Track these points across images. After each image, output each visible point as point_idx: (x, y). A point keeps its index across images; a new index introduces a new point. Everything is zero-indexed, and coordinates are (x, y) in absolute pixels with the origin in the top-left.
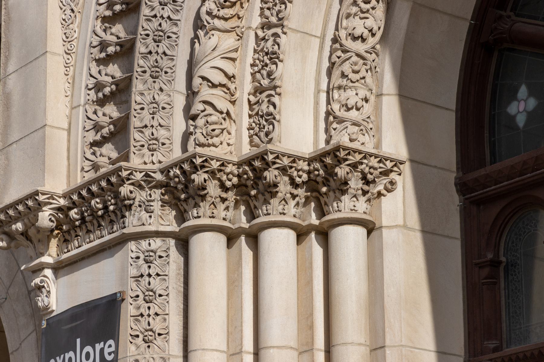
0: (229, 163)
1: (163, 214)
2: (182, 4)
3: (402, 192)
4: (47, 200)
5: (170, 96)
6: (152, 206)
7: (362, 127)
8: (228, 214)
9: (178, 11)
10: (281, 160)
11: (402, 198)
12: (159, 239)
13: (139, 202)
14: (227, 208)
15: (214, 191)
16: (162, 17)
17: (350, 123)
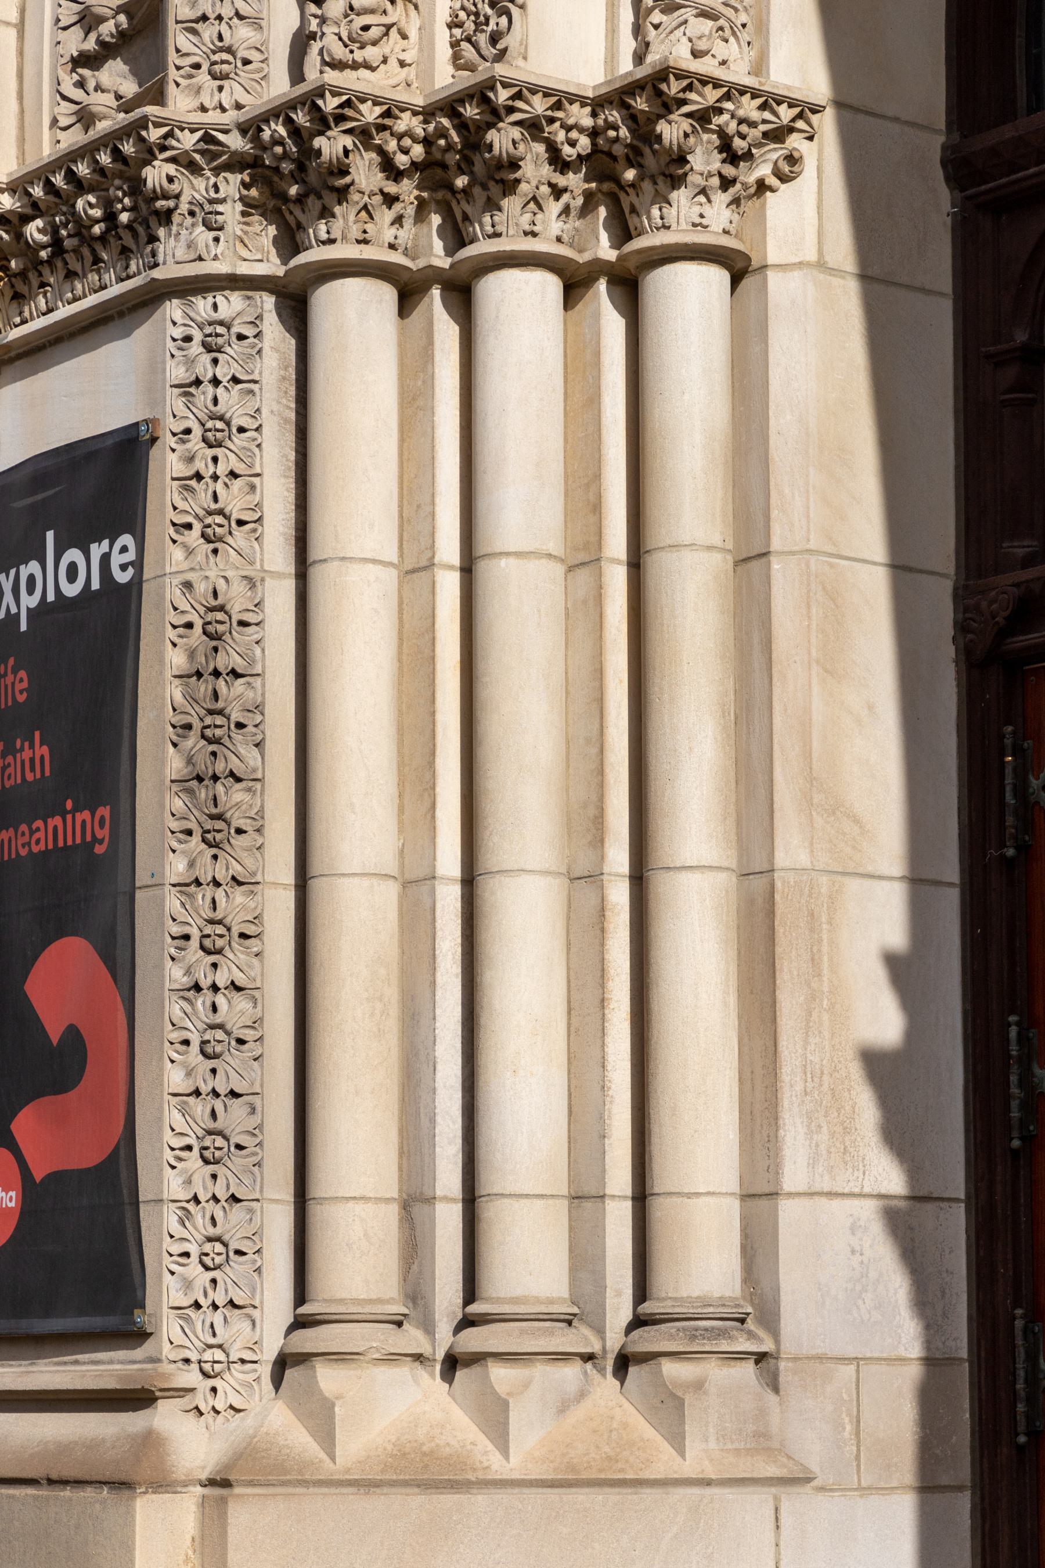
1: (246, 233)
3: (816, 181)
7: (722, 22)
8: (401, 233)
10: (527, 102)
12: (237, 293)
13: (190, 203)
14: (398, 220)
15: (367, 178)
17: (694, 12)
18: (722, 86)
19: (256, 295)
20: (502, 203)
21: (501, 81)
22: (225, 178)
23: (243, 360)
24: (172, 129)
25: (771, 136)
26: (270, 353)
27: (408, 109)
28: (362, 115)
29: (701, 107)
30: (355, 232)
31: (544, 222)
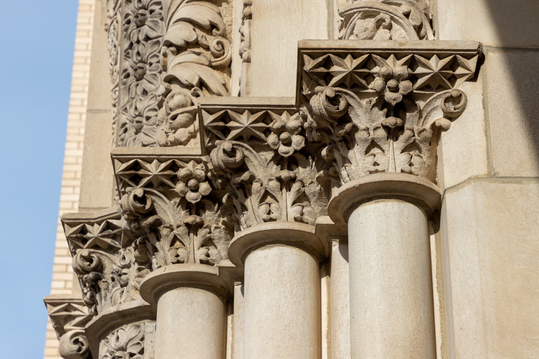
0: (187, 162)
3: (482, 111)
6: (125, 274)
7: (382, 15)
8: (212, 251)
11: (483, 122)
12: (130, 325)
13: (112, 273)
14: (208, 242)
15: (174, 217)
17: (359, 16)
18: (362, 54)
19: (141, 323)
21: (205, 109)
22: (129, 250)
24: (84, 225)
25: (434, 85)
27: (191, 159)
28: (149, 171)
29: (343, 75)
30: (171, 258)
31: (278, 209)
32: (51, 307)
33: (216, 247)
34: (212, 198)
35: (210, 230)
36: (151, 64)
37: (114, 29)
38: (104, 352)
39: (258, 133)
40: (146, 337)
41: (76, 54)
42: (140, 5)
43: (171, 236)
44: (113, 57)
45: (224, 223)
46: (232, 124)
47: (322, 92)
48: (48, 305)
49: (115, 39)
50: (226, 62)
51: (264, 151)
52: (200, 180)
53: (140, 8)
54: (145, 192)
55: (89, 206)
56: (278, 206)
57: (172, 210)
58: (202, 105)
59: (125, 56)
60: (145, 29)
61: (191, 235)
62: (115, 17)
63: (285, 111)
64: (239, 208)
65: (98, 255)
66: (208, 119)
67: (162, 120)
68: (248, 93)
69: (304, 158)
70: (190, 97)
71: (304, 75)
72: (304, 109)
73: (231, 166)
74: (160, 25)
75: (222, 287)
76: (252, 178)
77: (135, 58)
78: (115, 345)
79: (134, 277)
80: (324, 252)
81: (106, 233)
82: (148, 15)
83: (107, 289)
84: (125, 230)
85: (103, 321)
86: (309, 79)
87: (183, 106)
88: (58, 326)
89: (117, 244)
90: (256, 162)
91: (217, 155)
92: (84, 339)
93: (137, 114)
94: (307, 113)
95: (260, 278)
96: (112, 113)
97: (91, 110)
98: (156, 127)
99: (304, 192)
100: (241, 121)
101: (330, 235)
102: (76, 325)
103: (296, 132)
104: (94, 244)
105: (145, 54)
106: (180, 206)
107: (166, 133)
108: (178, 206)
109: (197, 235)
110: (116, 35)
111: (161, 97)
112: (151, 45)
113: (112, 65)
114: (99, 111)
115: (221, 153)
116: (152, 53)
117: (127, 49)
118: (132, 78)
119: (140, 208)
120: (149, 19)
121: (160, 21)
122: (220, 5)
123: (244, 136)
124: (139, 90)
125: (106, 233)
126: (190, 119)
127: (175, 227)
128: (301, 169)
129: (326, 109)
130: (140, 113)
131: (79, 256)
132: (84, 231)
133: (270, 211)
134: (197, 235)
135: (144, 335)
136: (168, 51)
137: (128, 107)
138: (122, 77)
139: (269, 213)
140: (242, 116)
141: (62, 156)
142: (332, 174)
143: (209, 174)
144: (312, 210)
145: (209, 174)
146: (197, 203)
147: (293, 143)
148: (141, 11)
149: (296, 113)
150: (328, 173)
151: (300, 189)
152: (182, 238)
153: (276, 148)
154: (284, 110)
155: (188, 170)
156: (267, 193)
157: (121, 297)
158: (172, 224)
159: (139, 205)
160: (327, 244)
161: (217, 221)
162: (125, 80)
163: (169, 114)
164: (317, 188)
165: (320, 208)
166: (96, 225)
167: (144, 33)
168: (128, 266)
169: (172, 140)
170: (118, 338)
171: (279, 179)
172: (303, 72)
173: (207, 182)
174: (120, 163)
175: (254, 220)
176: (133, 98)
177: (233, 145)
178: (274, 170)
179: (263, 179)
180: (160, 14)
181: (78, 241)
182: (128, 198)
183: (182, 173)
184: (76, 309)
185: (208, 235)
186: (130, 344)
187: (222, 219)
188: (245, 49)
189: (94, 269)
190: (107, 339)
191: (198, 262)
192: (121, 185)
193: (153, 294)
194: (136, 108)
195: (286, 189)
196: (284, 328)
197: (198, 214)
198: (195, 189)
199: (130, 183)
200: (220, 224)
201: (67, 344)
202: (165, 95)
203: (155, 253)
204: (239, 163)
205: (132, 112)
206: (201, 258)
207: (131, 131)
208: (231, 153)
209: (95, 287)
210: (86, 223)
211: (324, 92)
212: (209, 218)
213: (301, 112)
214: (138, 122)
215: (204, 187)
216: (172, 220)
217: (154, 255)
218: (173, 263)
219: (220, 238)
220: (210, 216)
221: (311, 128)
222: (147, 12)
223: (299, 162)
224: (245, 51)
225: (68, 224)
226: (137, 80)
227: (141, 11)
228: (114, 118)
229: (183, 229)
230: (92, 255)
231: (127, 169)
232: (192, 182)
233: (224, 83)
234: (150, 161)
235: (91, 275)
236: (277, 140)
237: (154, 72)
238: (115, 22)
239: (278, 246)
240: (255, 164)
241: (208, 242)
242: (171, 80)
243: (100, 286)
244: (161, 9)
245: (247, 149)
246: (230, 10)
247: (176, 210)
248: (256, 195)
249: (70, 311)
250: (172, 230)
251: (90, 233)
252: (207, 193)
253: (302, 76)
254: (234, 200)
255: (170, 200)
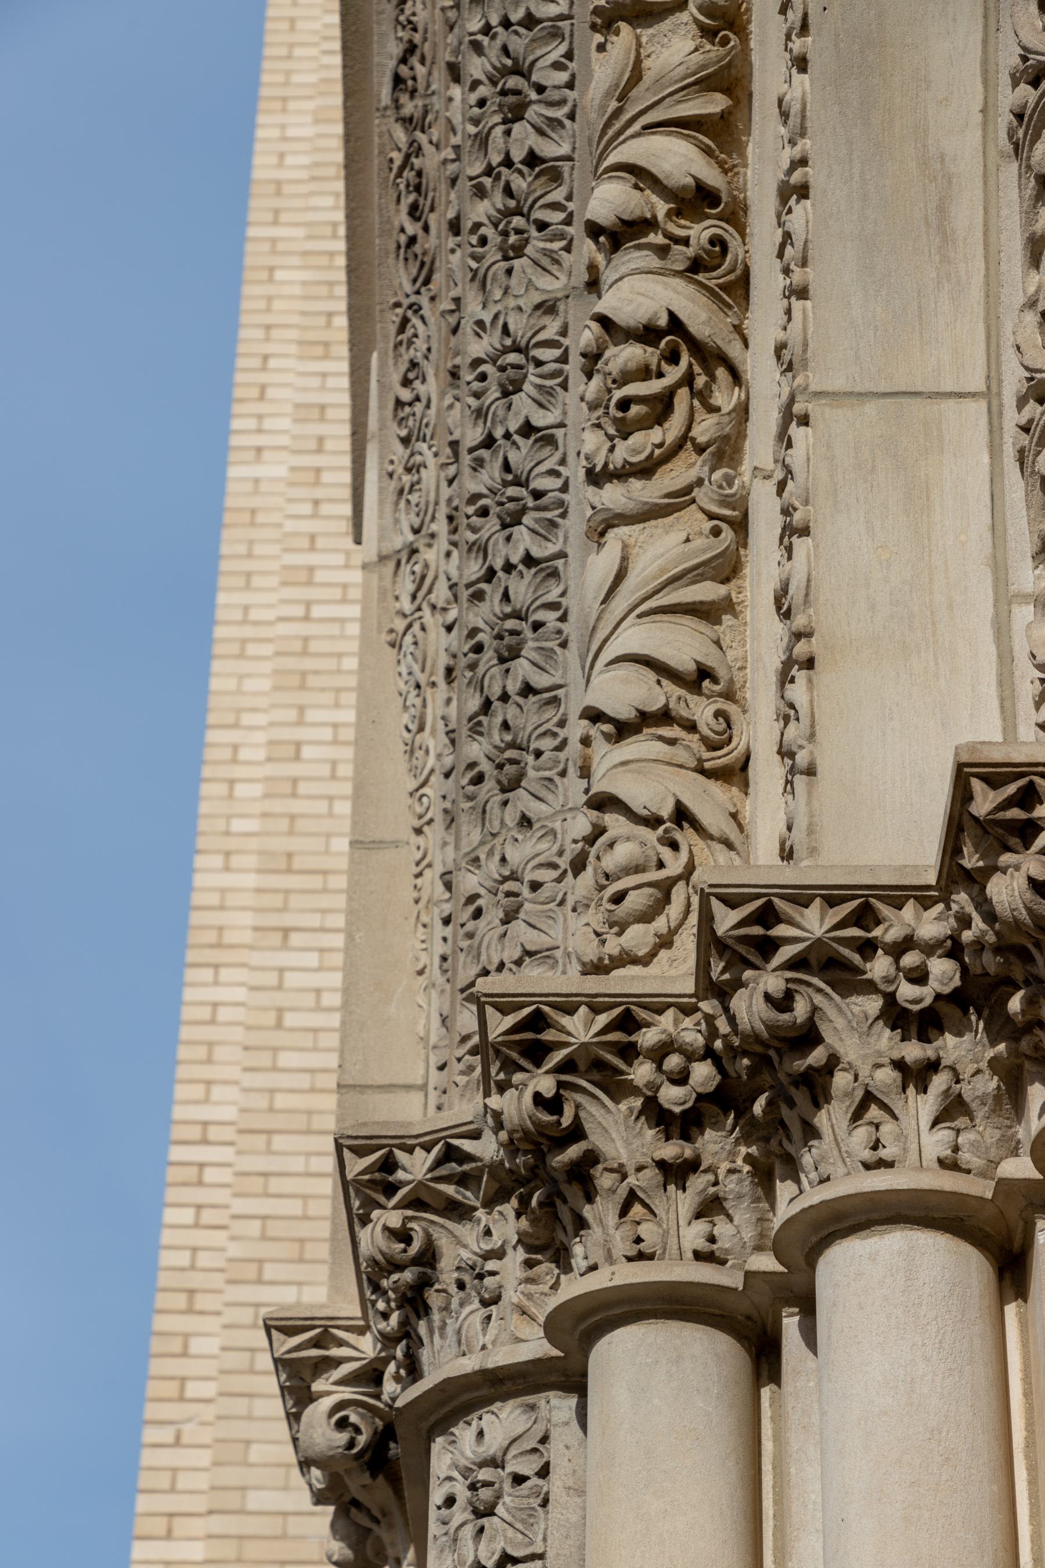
0: (660, 1010)
1: (529, 1296)
2: (564, 496)
4: (314, 1352)
5: (553, 832)
6: (493, 1273)
8: (723, 1229)
9: (553, 524)
10: (791, 922)
12: (511, 1403)
13: (458, 1268)
14: (711, 1207)
15: (627, 1143)
16: (509, 568)
19: (539, 1399)
20: (816, 1121)
22: (501, 1213)
23: (523, 1521)
24: (391, 1152)
26: (564, 1498)
27: (669, 1005)
28: (569, 1034)
30: (622, 1246)
32: (282, 1337)
33: (730, 1219)
34: (724, 1101)
35: (716, 1175)
36: (538, 754)
37: (416, 643)
38: (444, 1467)
39: (846, 952)
40: (554, 1434)
41: (219, 632)
42: (508, 610)
43: (622, 1192)
44: (413, 711)
45: (748, 1159)
46: (782, 930)
47: (1017, 868)
48: (274, 1332)
49: (416, 668)
50: (737, 759)
51: (859, 994)
52: (690, 1056)
53: (507, 617)
54: (560, 1085)
55: (362, 1082)
56: (897, 1130)
57: (622, 1128)
58: (711, 886)
59: (470, 730)
60: (522, 669)
61: (671, 1188)
62: (417, 615)
63: (912, 900)
64: (796, 1130)
65: (424, 1224)
66: (726, 920)
67: (585, 902)
68: (813, 851)
69: (958, 1013)
70: (654, 848)
71: (968, 823)
72: (962, 899)
73: (783, 1034)
74: (561, 659)
75: (749, 1318)
76: (833, 1062)
77: (497, 737)
78: (474, 1452)
79: (516, 1283)
80: (1010, 1239)
81: (442, 1171)
82: (528, 633)
83: (446, 1308)
84: (494, 1168)
85: (443, 1391)
86: (979, 832)
87: (638, 869)
88: (296, 1383)
89: (469, 1197)
90: (840, 1022)
91: (750, 1006)
92: (362, 1416)
93: (507, 873)
94: (970, 909)
95: (861, 1308)
96: (414, 848)
97: (361, 842)
98: (556, 909)
99: (960, 1095)
100: (805, 924)
101: (1031, 1204)
102: (340, 1382)
103: (940, 952)
104: (413, 1197)
105: (524, 728)
106: (643, 1118)
107: (598, 934)
108: (637, 1118)
109: (684, 1190)
110: (420, 660)
111: (580, 845)
112: (537, 706)
113: (409, 730)
114: (379, 844)
115: (760, 1005)
116: (540, 725)
117: (476, 715)
118: (489, 785)
119: (550, 1124)
120: (531, 644)
121: (558, 650)
122: (718, 622)
123: (813, 960)
124: (511, 817)
125: (442, 1171)
126: (657, 900)
127: (630, 1169)
128: (950, 1039)
129: (1029, 910)
130: (513, 872)
131: (379, 1228)
132: (389, 1165)
133: (878, 1141)
134: (684, 1190)
135: (547, 1430)
136: (595, 731)
137: (483, 857)
138: (465, 781)
139: (876, 1146)
140: (807, 911)
141: (188, 888)
142: (1028, 1053)
143: (718, 1044)
144: (979, 1138)
145: (718, 1044)
146: (684, 1112)
147: (931, 976)
148: (511, 624)
149: (936, 903)
150: (1017, 1050)
151: (949, 1088)
152: (649, 1196)
153: (891, 989)
154: (908, 898)
155: (664, 1031)
156: (869, 1098)
157: (484, 1330)
158: (624, 1161)
159: (547, 1118)
160: (1021, 1223)
161: (732, 1155)
162: (471, 788)
163: (602, 888)
164: (990, 1084)
165: (998, 1133)
166: (419, 1152)
167: (520, 678)
168: (499, 1254)
169: (615, 952)
170: (481, 1434)
171: (899, 1065)
172: (966, 817)
173: (709, 1061)
174: (498, 1014)
175: (840, 1163)
176: (494, 835)
177: (788, 981)
178: (886, 1041)
179: (858, 1063)
180: (559, 632)
181: (375, 1191)
182: (519, 1098)
183: (648, 1038)
184: (341, 1343)
185: (712, 1190)
186: (513, 1452)
187: (743, 1150)
188: (801, 742)
189: (416, 1261)
190: (453, 1434)
191: (690, 1255)
192: (498, 1064)
193: (578, 1333)
194: (503, 860)
195: (916, 1087)
196: (928, 1435)
197: (687, 1137)
198: (681, 1078)
199: (523, 1062)
200: (739, 1162)
201: (320, 1431)
202: (590, 840)
203: (582, 1233)
204: (802, 1025)
205: (493, 867)
206: (695, 1247)
207: (493, 915)
208: (783, 1003)
209: (415, 1302)
210: (395, 1146)
211: (1024, 868)
212: (712, 1148)
213: (955, 907)
214: (508, 894)
215: (703, 1073)
216: (622, 1151)
217: (576, 1235)
218: (630, 1259)
219: (740, 1197)
220: (715, 1143)
221: (979, 945)
222: (525, 627)
223: (946, 1022)
224: (801, 747)
225: (351, 1148)
226: (504, 790)
227: (511, 624)
228: (418, 864)
229: (651, 1176)
230: (409, 1225)
231: (515, 1029)
232: (673, 1061)
233: (733, 810)
234: (570, 1010)
235: (408, 1276)
236: (893, 971)
237: (547, 774)
238: (416, 627)
239: (902, 1229)
240: (839, 1027)
241: (711, 1207)
242: (603, 803)
243: (429, 1301)
244: (563, 619)
245: (819, 990)
246: (740, 633)
247: (633, 1128)
248: (842, 1102)
249: (326, 1348)
250: (624, 1177)
251: (405, 1170)
252: (711, 1088)
253: (959, 824)
254: (785, 1112)
255: (617, 1101)
